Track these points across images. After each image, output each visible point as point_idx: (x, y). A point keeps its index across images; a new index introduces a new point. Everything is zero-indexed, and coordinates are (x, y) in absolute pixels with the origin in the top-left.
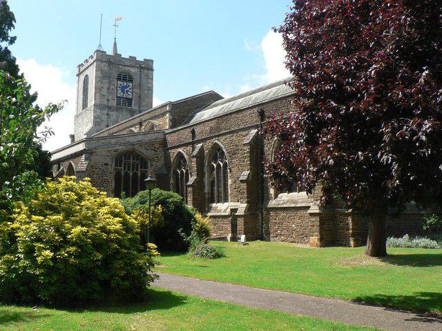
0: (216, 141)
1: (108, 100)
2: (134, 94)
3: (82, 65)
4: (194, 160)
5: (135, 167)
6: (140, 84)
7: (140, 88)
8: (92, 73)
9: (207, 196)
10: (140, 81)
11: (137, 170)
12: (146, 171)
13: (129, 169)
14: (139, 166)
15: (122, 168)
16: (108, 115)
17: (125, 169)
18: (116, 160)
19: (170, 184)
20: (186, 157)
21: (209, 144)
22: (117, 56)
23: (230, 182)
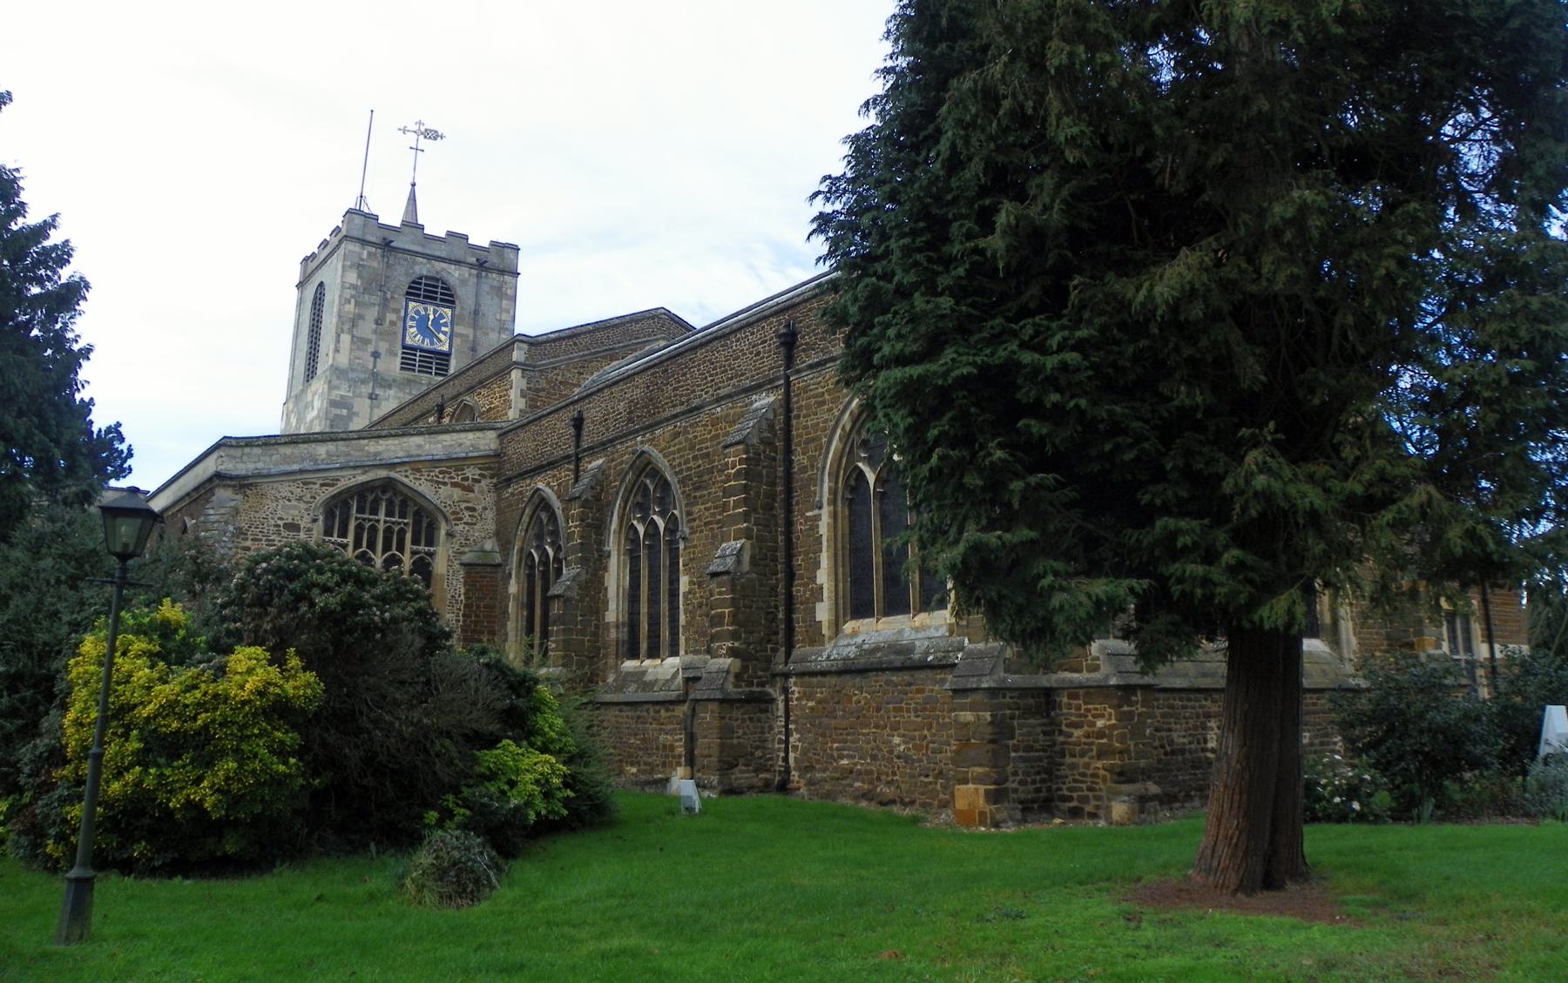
0: (646, 447)
1: (376, 355)
2: (457, 341)
3: (313, 256)
4: (575, 511)
5: (393, 539)
6: (476, 312)
7: (475, 326)
8: (333, 276)
9: (613, 634)
10: (477, 304)
11: (401, 548)
12: (431, 555)
13: (372, 545)
14: (409, 536)
15: (350, 539)
16: (372, 397)
17: (357, 544)
18: (329, 516)
19: (507, 597)
20: (557, 505)
21: (624, 453)
22: (412, 224)
23: (684, 582)
